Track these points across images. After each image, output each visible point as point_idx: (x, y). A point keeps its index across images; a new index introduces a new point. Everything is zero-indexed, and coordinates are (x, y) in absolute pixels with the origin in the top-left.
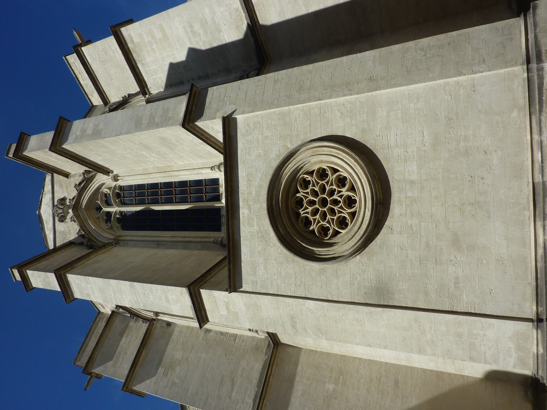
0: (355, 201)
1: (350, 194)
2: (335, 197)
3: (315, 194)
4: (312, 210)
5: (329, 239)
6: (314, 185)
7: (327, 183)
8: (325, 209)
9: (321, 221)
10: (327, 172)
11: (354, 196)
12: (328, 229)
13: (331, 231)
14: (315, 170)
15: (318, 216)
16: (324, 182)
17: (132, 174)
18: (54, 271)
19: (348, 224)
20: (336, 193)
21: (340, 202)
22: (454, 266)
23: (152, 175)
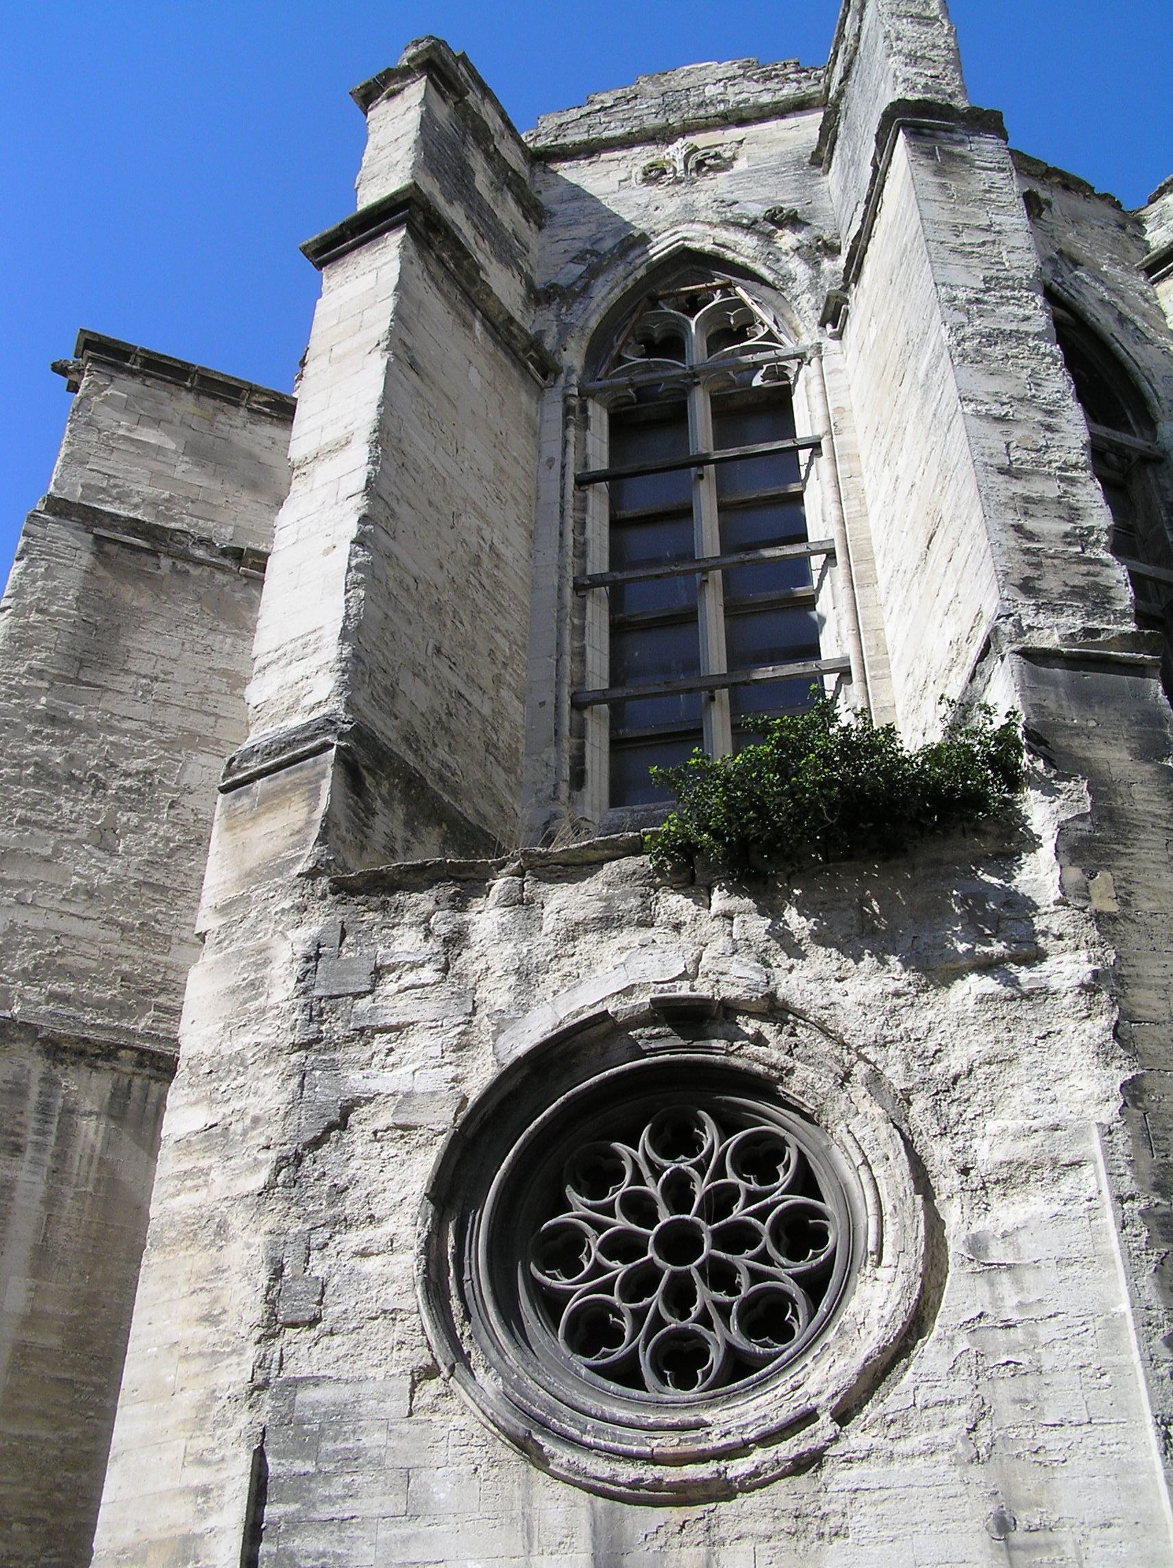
0: (685, 1382)
1: (716, 1357)
2: (704, 1295)
3: (720, 1202)
4: (647, 1197)
5: (535, 1287)
6: (752, 1197)
7: (764, 1257)
8: (651, 1254)
9: (602, 1236)
10: (811, 1251)
11: (706, 1375)
12: (572, 1269)
13: (562, 1283)
14: (823, 1201)
15: (621, 1222)
16: (766, 1239)
17: (869, 648)
18: (415, 184)
19: (590, 1357)
20: (722, 1297)
21: (684, 1315)
22: (297, 1079)
23: (847, 591)
